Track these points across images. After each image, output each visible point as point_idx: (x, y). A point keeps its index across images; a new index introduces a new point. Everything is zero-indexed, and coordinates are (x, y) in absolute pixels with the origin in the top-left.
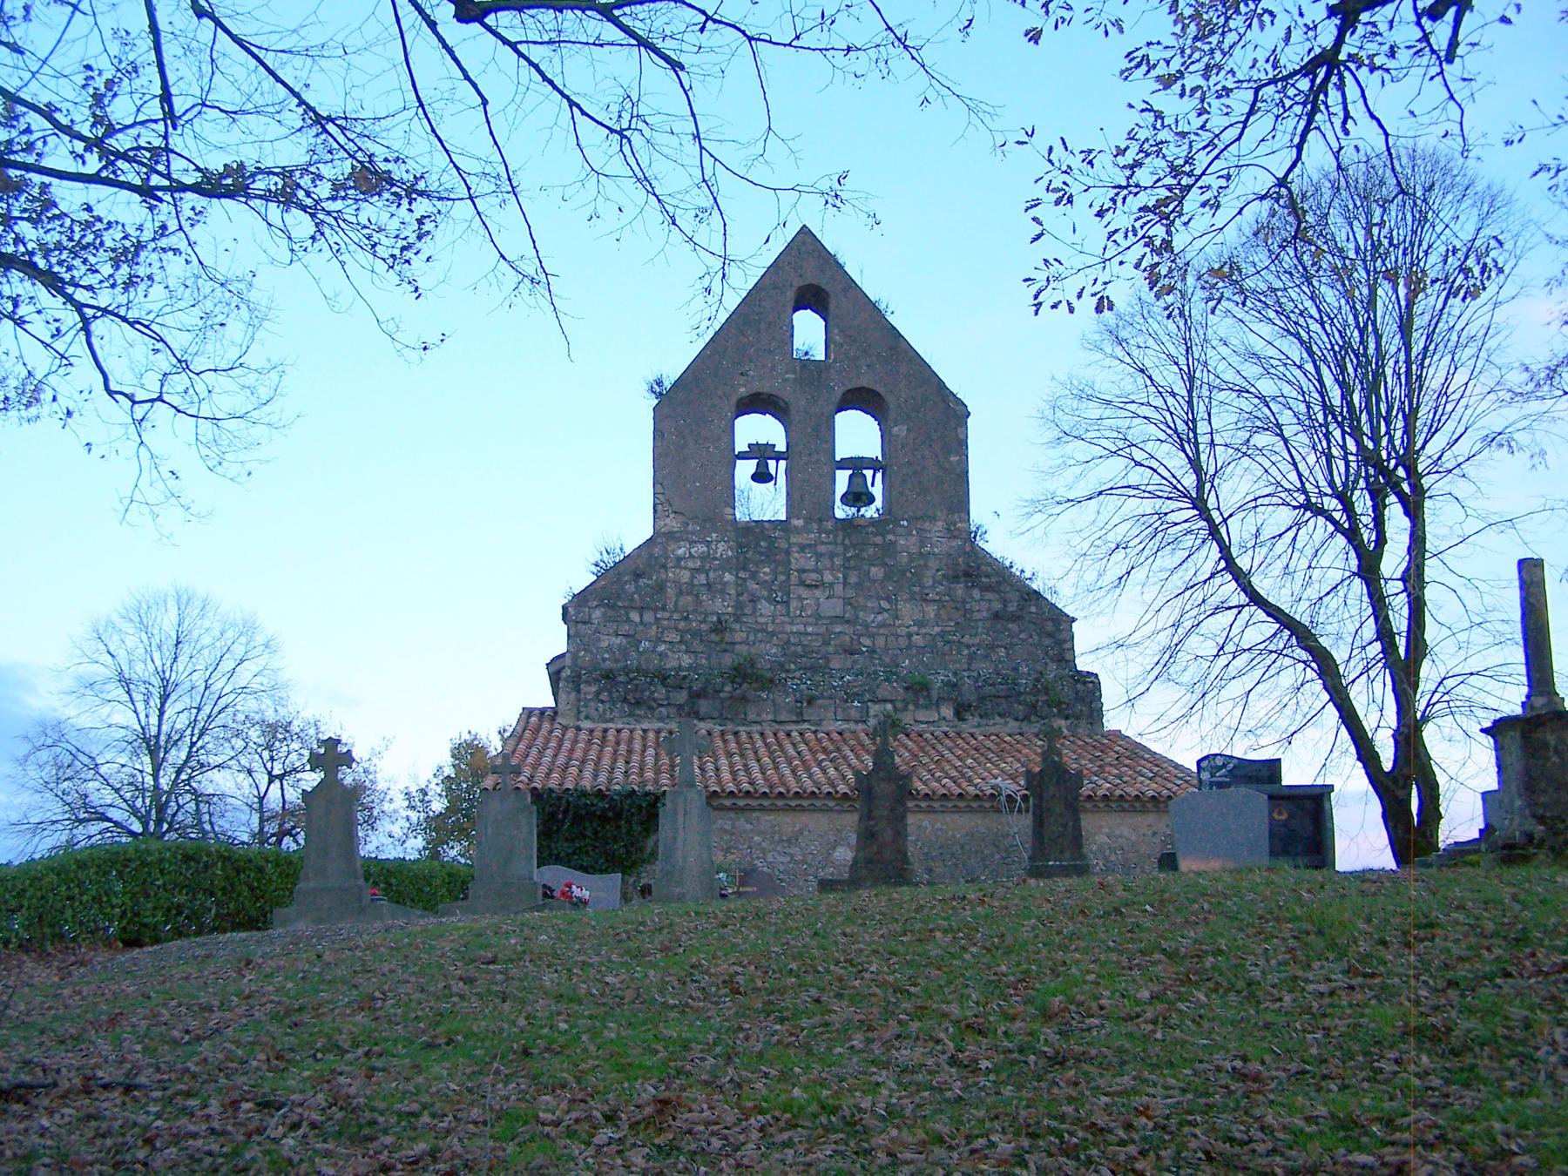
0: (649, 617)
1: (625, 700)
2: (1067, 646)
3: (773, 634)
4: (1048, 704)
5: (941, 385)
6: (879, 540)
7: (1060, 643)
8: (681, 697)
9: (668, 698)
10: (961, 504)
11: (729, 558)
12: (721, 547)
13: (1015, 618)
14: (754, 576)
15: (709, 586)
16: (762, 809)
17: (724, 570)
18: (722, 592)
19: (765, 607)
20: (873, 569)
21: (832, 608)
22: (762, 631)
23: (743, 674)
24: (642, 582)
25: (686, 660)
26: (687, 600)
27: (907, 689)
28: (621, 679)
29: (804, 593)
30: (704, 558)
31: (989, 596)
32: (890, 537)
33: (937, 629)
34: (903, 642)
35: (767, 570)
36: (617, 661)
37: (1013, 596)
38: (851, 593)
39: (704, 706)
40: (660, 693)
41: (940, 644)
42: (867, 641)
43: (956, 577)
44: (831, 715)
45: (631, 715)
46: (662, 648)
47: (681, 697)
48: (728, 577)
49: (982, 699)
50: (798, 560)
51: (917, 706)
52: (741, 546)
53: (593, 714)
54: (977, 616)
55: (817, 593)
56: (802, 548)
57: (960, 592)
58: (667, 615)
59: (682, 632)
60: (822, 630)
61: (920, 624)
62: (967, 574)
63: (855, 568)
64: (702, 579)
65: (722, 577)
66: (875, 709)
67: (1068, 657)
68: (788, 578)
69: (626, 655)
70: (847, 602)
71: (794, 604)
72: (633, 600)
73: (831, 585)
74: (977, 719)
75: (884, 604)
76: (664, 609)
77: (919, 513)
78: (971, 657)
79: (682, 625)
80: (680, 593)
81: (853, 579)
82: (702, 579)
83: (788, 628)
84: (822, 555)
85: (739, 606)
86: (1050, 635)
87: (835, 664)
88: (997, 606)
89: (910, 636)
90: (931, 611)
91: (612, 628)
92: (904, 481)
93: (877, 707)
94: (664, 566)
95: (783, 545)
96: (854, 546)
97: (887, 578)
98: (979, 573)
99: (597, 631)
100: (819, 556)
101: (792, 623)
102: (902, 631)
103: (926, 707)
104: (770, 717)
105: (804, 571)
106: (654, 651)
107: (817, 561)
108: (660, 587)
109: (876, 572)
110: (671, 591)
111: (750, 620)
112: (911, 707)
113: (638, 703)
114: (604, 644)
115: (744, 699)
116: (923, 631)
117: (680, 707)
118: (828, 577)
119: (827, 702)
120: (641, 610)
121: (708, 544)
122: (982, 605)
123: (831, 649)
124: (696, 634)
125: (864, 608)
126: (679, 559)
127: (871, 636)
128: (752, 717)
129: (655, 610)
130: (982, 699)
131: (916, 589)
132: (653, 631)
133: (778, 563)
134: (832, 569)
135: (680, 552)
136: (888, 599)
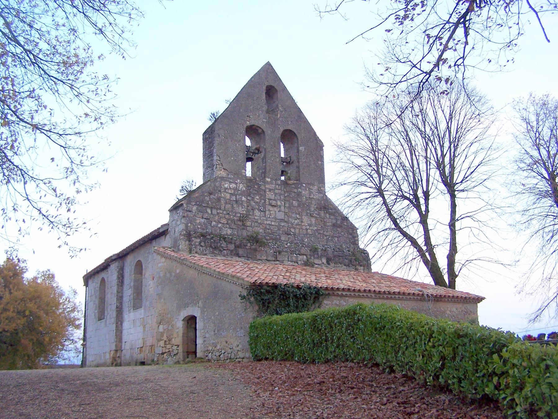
0: (214, 212)
1: (211, 246)
2: (356, 239)
3: (260, 224)
4: (355, 260)
5: (315, 133)
6: (296, 191)
7: (354, 237)
8: (232, 247)
9: (227, 247)
10: (321, 180)
11: (244, 191)
12: (241, 186)
13: (340, 227)
14: (253, 198)
15: (236, 201)
16: (350, 296)
17: (241, 194)
18: (242, 204)
19: (257, 213)
20: (294, 202)
21: (281, 215)
22: (257, 222)
23: (255, 239)
24: (212, 196)
25: (229, 232)
26: (228, 206)
27: (310, 250)
28: (208, 237)
29: (271, 208)
30: (236, 189)
31: (332, 217)
32: (299, 190)
33: (316, 228)
34: (305, 232)
35: (257, 197)
36: (203, 229)
37: (339, 218)
38: (287, 211)
39: (241, 251)
40: (224, 244)
41: (317, 234)
42: (293, 230)
43: (321, 208)
44: (286, 259)
45: (213, 253)
46: (220, 225)
47: (232, 247)
48: (244, 199)
49: (335, 256)
50: (269, 195)
51: (314, 258)
52: (248, 186)
53: (199, 251)
54: (328, 224)
55: (275, 209)
56: (270, 190)
57: (322, 214)
58: (221, 212)
59: (228, 220)
60: (277, 224)
61: (310, 225)
62: (325, 208)
63: (288, 201)
64: (234, 198)
65: (241, 198)
66: (300, 257)
67: (357, 243)
68: (265, 202)
69: (207, 227)
70: (286, 214)
71: (267, 212)
72: (208, 204)
73: (280, 206)
74: (333, 264)
75: (298, 216)
76: (220, 209)
77: (309, 182)
78: (327, 239)
79: (227, 216)
80: (226, 203)
81: (287, 205)
82: (234, 198)
83: (265, 222)
84: (277, 194)
85: (248, 211)
86: (351, 234)
87: (283, 238)
88: (334, 221)
89: (307, 230)
90: (313, 220)
91: (200, 215)
92: (304, 169)
93: (301, 257)
94: (220, 191)
95: (263, 188)
96: (287, 192)
97: (299, 206)
98: (327, 207)
99: (195, 215)
100: (276, 194)
101: (267, 220)
102: (304, 227)
103: (318, 258)
104: (265, 258)
105: (271, 200)
106: (217, 226)
107: (275, 196)
108: (219, 200)
109: (295, 203)
110: (223, 202)
111: (252, 217)
112: (312, 258)
113: (215, 248)
114: (198, 221)
115: (255, 250)
116: (311, 228)
117: (231, 251)
118: (279, 203)
119: (285, 253)
120: (211, 208)
121: (236, 184)
122: (330, 221)
123: (281, 232)
124: (233, 221)
125: (291, 217)
126: (226, 189)
127: (295, 228)
128: (258, 257)
129: (217, 209)
130: (335, 256)
131: (309, 212)
132: (217, 218)
133: (261, 195)
134: (280, 200)
135: (226, 186)
136: (299, 214)
